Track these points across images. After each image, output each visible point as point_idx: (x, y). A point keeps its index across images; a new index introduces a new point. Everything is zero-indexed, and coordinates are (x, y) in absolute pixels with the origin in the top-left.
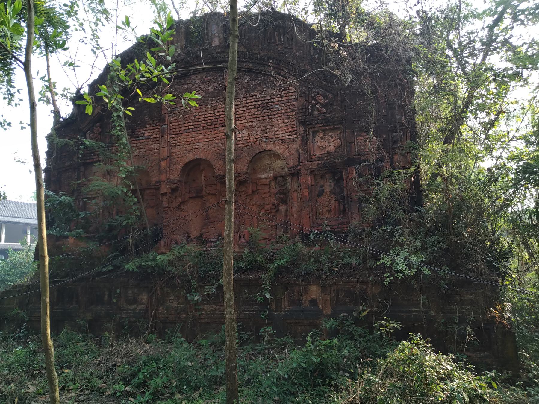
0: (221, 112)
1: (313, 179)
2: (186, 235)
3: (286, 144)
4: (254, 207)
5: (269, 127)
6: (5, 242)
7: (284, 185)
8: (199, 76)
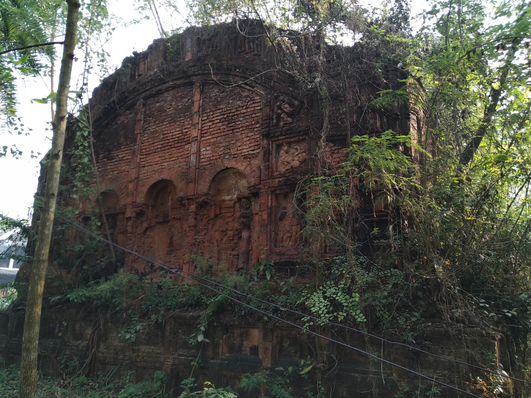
0: (188, 128)
1: (274, 199)
2: (150, 265)
3: (248, 159)
4: (217, 233)
5: (232, 142)
6: (14, 267)
7: (249, 207)
8: (171, 92)
